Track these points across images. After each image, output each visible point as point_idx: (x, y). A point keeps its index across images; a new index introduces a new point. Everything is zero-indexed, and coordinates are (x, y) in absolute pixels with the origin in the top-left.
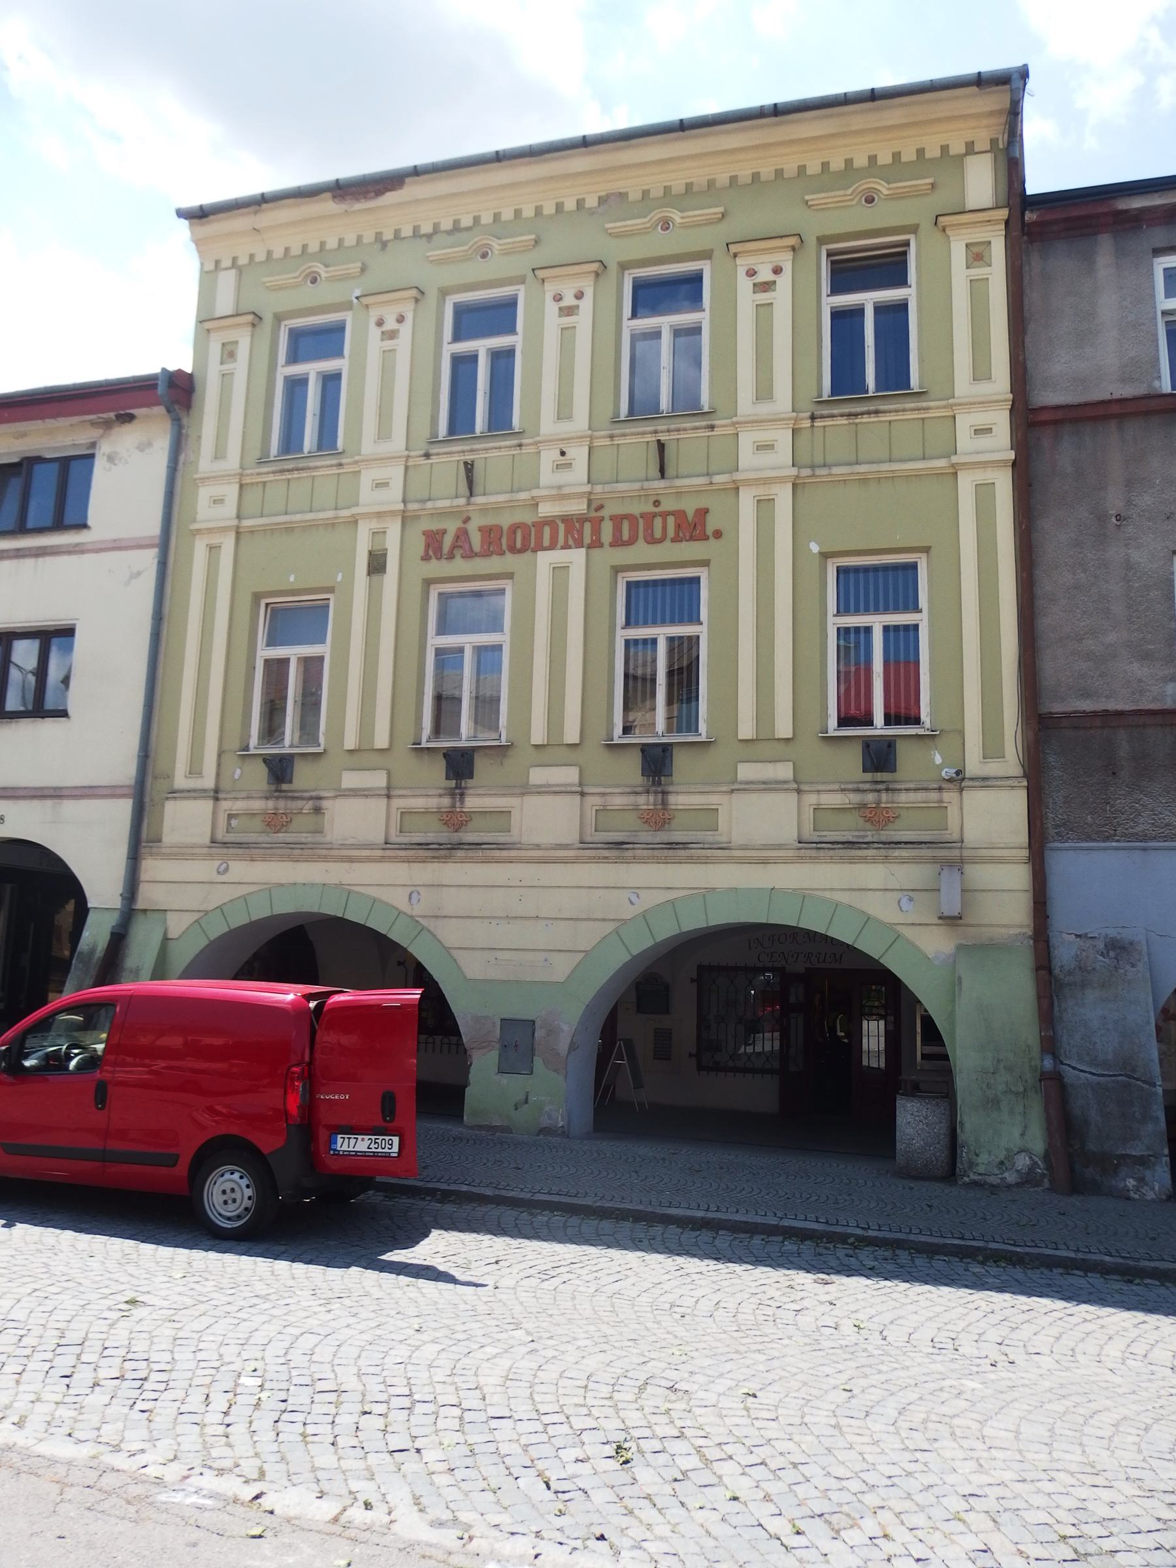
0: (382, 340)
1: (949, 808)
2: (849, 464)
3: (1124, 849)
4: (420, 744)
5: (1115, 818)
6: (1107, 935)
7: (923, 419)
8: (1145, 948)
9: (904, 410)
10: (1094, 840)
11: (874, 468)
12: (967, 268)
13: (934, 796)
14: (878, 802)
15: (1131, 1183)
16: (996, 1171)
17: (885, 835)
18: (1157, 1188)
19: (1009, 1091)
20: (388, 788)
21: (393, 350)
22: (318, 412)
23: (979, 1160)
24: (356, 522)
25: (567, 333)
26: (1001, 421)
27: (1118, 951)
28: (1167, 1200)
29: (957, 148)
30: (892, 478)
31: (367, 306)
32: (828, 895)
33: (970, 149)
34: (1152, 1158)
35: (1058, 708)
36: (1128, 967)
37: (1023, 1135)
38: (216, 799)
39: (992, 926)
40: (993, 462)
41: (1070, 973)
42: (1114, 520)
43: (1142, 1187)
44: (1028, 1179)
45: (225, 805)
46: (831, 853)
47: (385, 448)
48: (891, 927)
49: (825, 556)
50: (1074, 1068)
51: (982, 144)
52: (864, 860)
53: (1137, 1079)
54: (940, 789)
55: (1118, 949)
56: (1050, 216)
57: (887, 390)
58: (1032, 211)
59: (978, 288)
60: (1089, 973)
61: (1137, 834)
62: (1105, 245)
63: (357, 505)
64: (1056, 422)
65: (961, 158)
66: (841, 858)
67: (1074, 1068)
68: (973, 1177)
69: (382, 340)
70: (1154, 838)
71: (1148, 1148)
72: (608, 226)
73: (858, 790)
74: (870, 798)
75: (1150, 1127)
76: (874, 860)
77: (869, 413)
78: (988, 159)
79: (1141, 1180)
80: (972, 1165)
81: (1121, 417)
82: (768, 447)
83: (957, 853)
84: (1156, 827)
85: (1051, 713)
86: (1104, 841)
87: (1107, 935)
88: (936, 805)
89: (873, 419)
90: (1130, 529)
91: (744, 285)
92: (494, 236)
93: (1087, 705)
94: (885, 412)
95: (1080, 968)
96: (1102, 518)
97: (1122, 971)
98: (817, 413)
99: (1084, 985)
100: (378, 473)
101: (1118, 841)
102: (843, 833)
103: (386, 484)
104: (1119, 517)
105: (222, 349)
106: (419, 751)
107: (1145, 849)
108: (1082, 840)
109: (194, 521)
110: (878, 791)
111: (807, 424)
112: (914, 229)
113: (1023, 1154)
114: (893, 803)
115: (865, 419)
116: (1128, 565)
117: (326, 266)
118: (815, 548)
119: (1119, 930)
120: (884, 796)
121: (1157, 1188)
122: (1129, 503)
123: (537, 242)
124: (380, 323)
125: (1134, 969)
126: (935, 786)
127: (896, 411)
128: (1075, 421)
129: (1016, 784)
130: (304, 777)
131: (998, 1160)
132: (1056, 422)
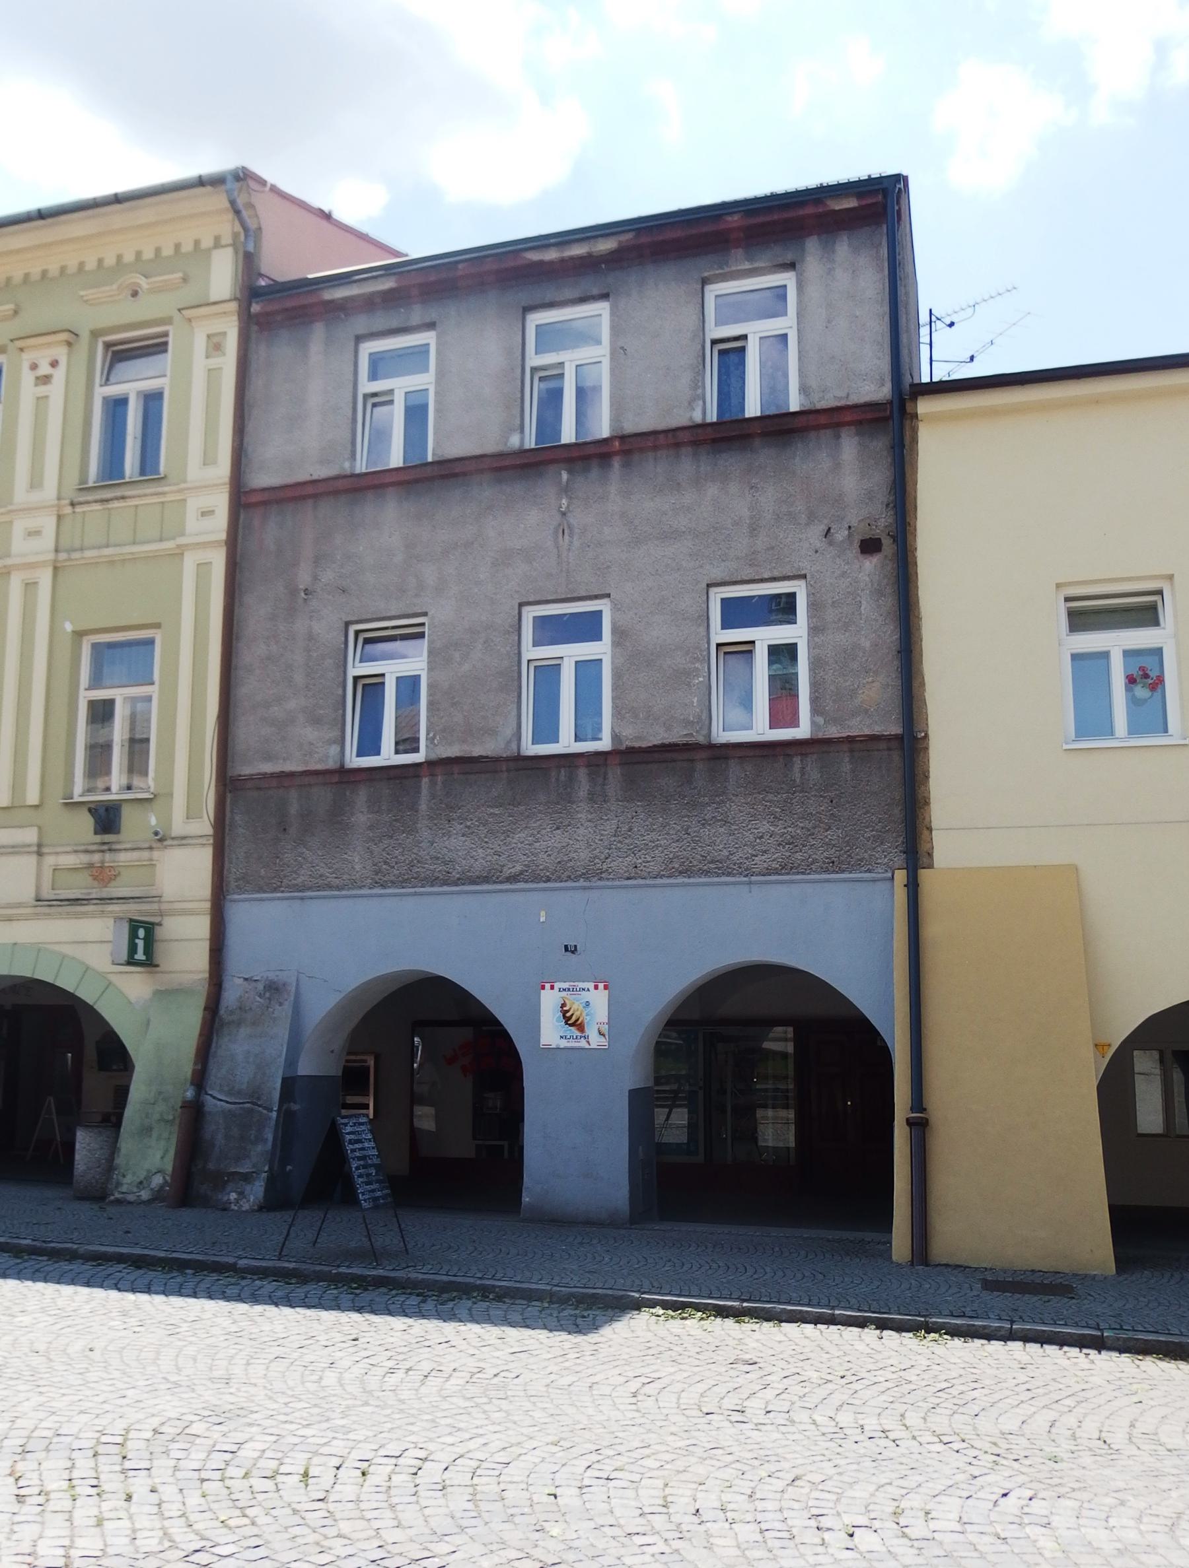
0: (36, 385)
1: (158, 865)
2: (99, 547)
3: (287, 899)
4: (72, 798)
5: (282, 871)
6: (267, 977)
7: (163, 503)
8: (294, 989)
9: (145, 495)
10: (265, 892)
11: (118, 550)
12: (207, 357)
13: (145, 854)
14: (103, 862)
15: (233, 1196)
16: (135, 1190)
17: (105, 893)
18: (252, 1200)
19: (162, 1120)
20: (39, 845)
21: (47, 397)
22: (139, 435)
23: (125, 1181)
24: (9, 573)
25: (42, 400)
26: (221, 502)
27: (273, 991)
28: (257, 1211)
29: (207, 242)
30: (134, 559)
31: (190, 320)
32: (57, 948)
33: (217, 244)
34: (254, 1175)
35: (247, 770)
36: (277, 1007)
37: (162, 1158)
38: (40, 854)
39: (181, 972)
40: (209, 542)
41: (232, 1012)
42: (302, 594)
43: (241, 1200)
44: (158, 1196)
45: (50, 860)
46: (60, 909)
47: (35, 497)
48: (102, 975)
49: (79, 634)
50: (214, 1098)
51: (227, 239)
52: (84, 915)
53: (259, 1106)
54: (151, 848)
55: (273, 989)
56: (270, 308)
57: (111, 479)
58: (257, 303)
59: (213, 375)
60: (246, 1012)
61: (297, 885)
62: (318, 331)
63: (183, 534)
64: (264, 503)
65: (209, 250)
66: (68, 913)
67: (214, 1098)
68: (117, 1195)
69: (36, 385)
70: (310, 889)
71: (254, 1166)
72: (82, 293)
73: (87, 851)
74: (96, 858)
75: (259, 1148)
76: (92, 915)
77: (117, 498)
78: (230, 250)
79: (241, 1194)
80: (119, 1184)
81: (315, 496)
82: (37, 533)
83: (155, 906)
84: (314, 878)
85: (240, 776)
86: (272, 892)
87: (267, 977)
88: (148, 863)
89: (122, 504)
90: (314, 603)
91: (28, 378)
92: (142, 275)
93: (268, 768)
94: (130, 497)
95: (240, 1008)
96: (293, 592)
97: (272, 1010)
98: (76, 500)
99: (239, 1023)
100: (32, 523)
101: (283, 892)
102: (74, 891)
103: (211, 512)
104: (306, 592)
105: (208, 342)
106: (72, 805)
107: (302, 899)
108: (258, 892)
109: (8, 555)
110: (103, 851)
111: (68, 510)
112: (168, 321)
113: (159, 1174)
114: (114, 862)
115: (116, 504)
116: (311, 637)
117: (146, 277)
118: (69, 627)
119: (278, 973)
120: (108, 856)
121: (252, 1200)
122: (315, 578)
123: (16, 312)
124: (34, 367)
125: (280, 1008)
126: (147, 845)
127: (139, 496)
128: (279, 502)
129: (205, 842)
130: (134, 824)
131: (139, 1180)
132: (264, 503)
